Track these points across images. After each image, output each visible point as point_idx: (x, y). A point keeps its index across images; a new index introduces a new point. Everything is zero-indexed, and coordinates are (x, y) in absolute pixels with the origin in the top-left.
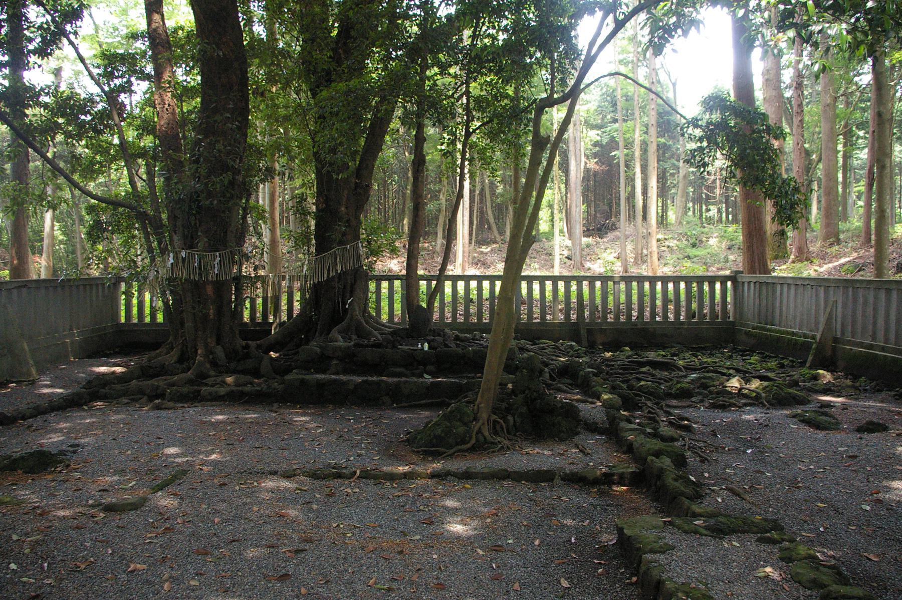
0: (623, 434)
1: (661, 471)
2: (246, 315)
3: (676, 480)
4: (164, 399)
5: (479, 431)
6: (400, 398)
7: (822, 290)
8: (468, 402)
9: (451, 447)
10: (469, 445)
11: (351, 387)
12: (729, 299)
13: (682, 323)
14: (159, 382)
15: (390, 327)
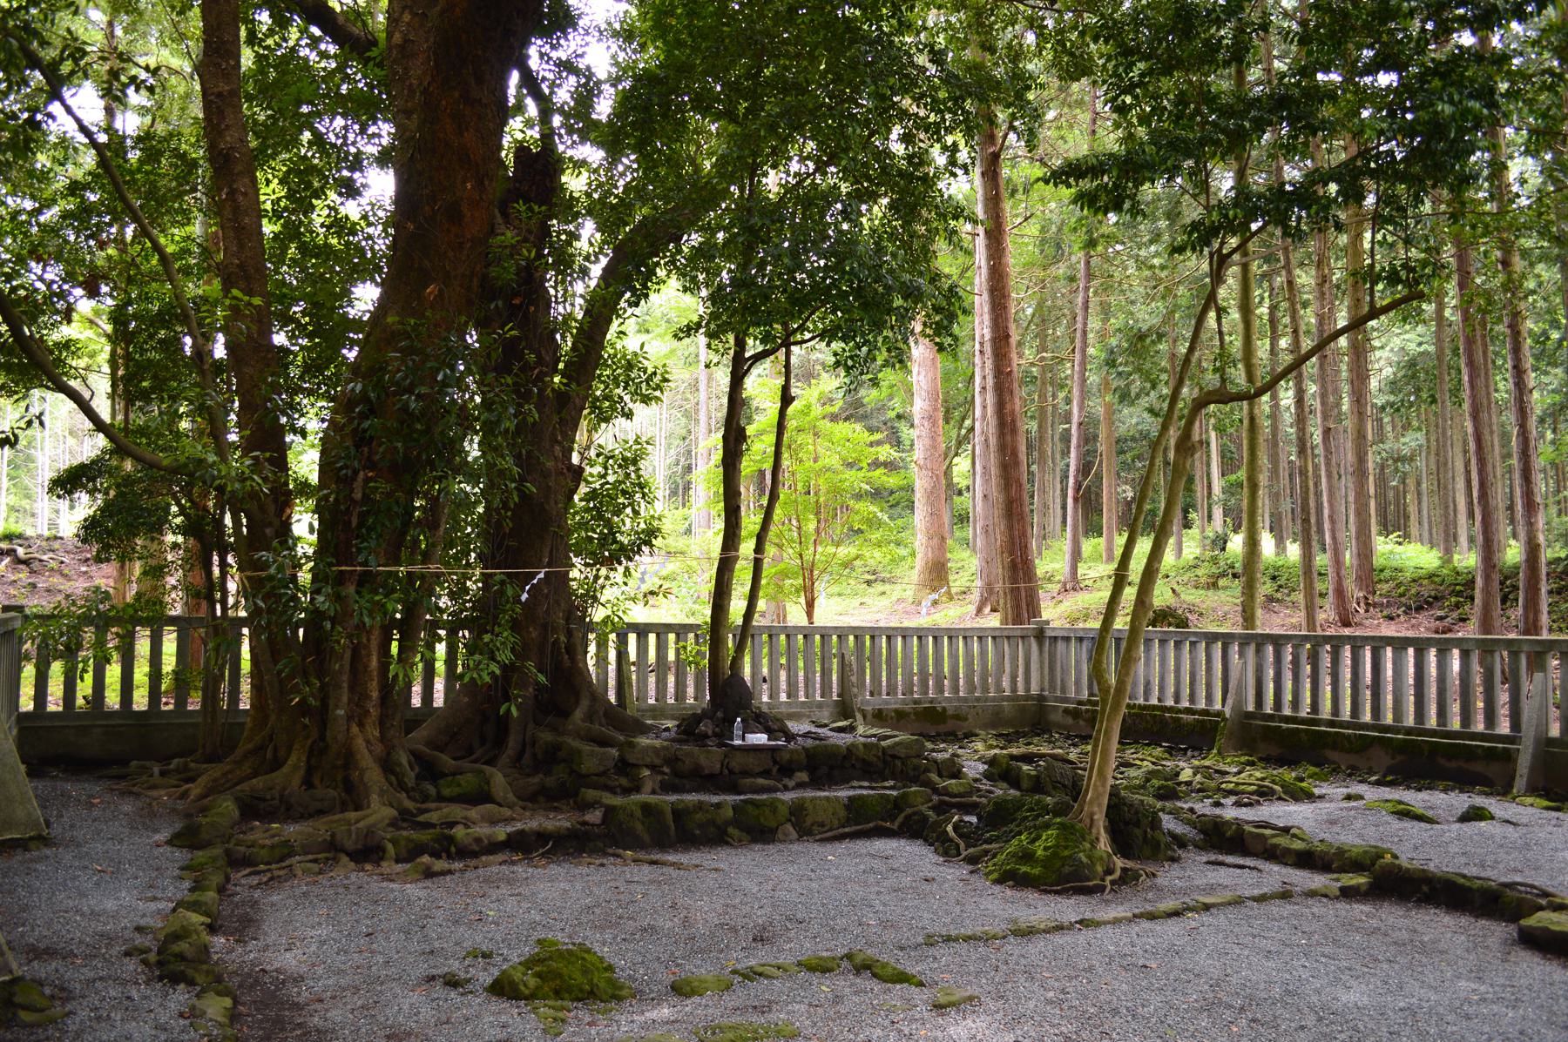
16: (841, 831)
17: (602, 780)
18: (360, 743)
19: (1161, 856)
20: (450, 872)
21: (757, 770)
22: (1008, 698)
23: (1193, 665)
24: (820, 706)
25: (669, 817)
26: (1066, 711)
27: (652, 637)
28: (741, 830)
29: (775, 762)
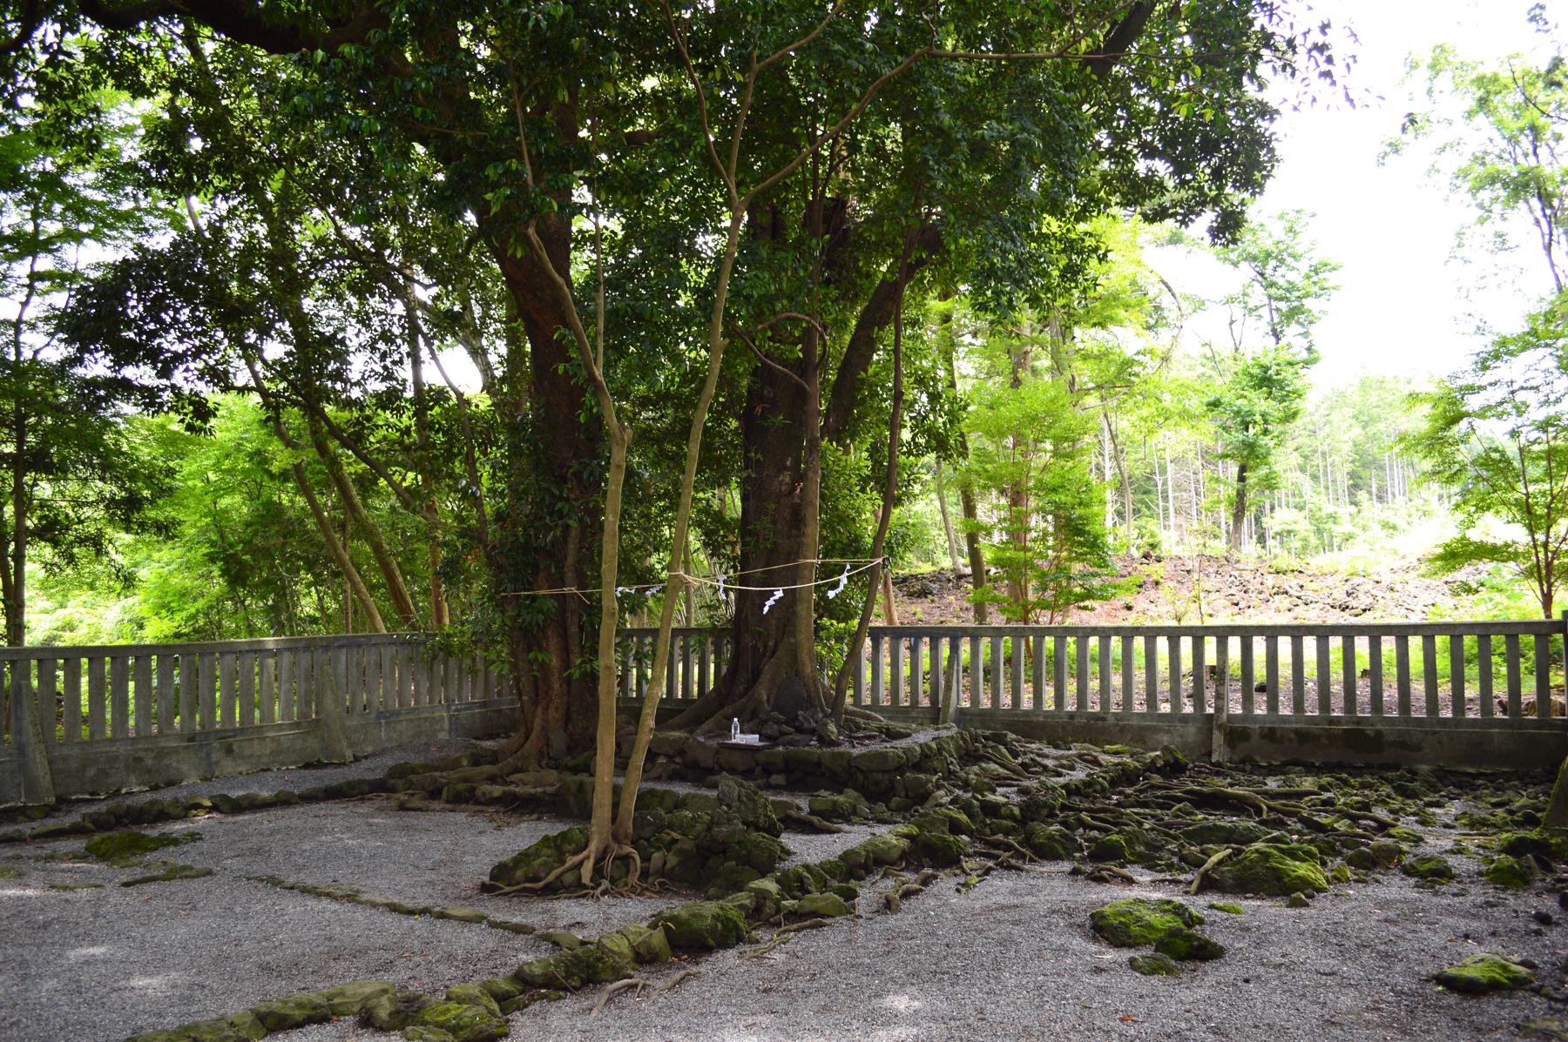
10: (541, 884)
12: (680, 666)
20: (420, 809)
24: (1185, 719)
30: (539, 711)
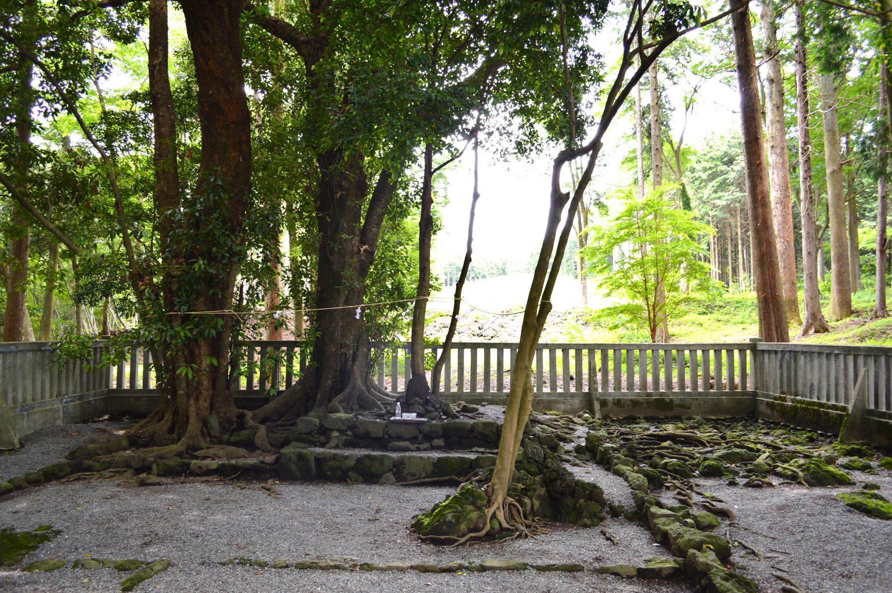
0: (657, 521)
1: (708, 567)
2: (243, 382)
3: (727, 580)
4: (150, 473)
5: (494, 516)
6: (403, 476)
7: (851, 359)
8: (479, 481)
9: (464, 535)
10: (484, 532)
11: (352, 463)
12: (748, 371)
13: (700, 394)
14: (151, 454)
15: (393, 397)
16: (427, 480)
17: (308, 437)
18: (192, 410)
19: (580, 522)
20: (159, 484)
21: (408, 436)
22: (726, 394)
23: (837, 373)
24: (573, 395)
25: (313, 464)
26: (768, 404)
27: (724, 352)
28: (359, 474)
29: (421, 433)
30: (192, 402)
